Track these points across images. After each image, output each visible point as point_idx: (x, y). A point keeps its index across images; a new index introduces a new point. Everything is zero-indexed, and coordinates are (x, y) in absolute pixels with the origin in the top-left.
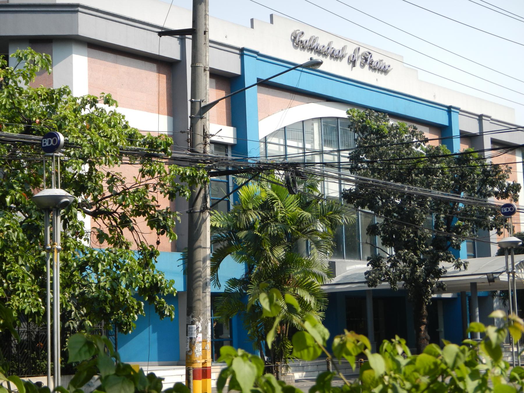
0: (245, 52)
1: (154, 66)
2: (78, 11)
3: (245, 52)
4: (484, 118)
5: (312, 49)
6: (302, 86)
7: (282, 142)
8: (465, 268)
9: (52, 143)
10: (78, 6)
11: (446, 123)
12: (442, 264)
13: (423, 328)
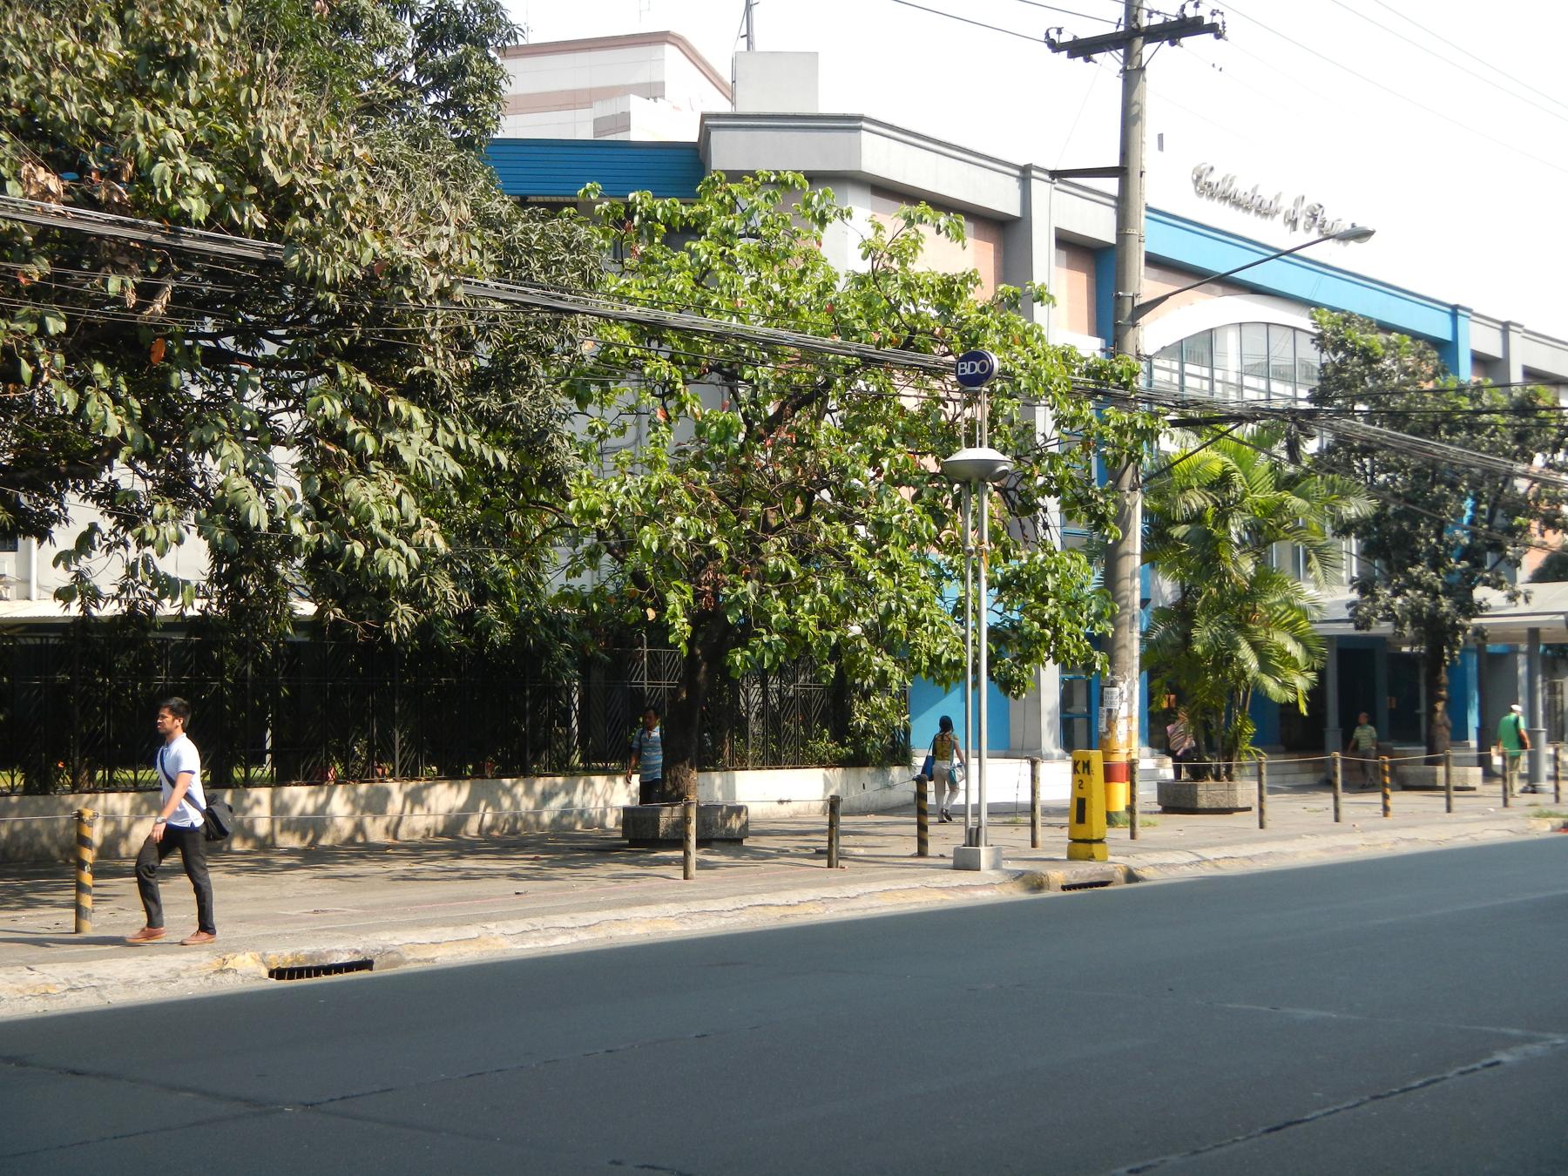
2: (860, 128)
4: (1034, 173)
5: (1225, 198)
7: (1176, 366)
8: (1527, 600)
9: (977, 369)
10: (861, 118)
11: (1498, 353)
12: (1480, 593)
13: (1440, 706)
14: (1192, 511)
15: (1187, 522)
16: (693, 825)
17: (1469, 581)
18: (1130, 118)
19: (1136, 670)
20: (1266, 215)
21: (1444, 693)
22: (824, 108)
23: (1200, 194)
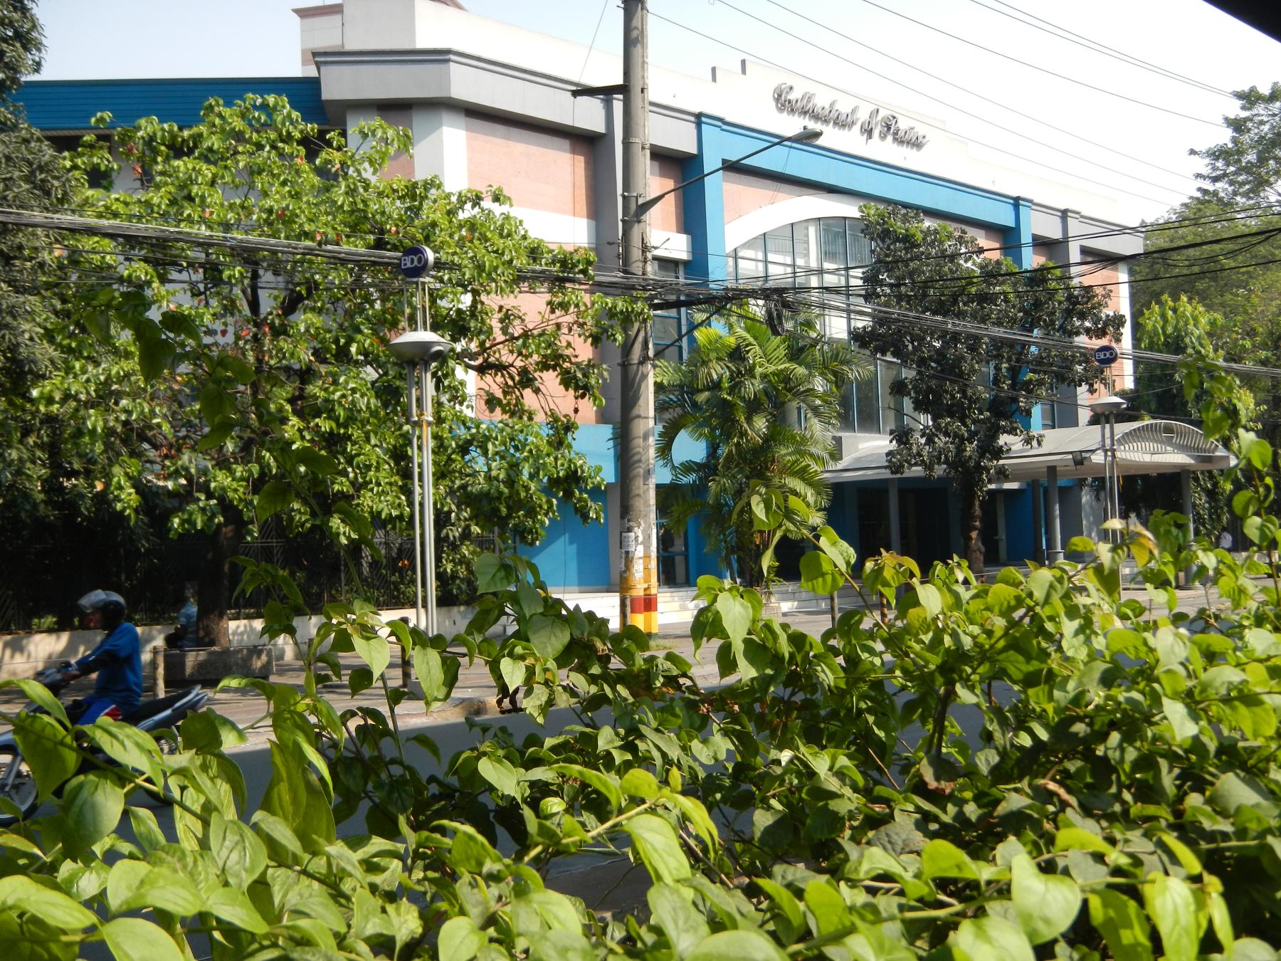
0: (703, 119)
1: (566, 143)
3: (703, 119)
6: (790, 171)
7: (760, 256)
8: (1039, 444)
9: (415, 262)
10: (448, 52)
12: (1004, 439)
13: (974, 534)
14: (712, 381)
15: (708, 389)
16: (161, 671)
17: (995, 432)
18: (632, 41)
19: (653, 516)
20: (843, 126)
21: (977, 523)
22: (421, 44)
23: (780, 110)
